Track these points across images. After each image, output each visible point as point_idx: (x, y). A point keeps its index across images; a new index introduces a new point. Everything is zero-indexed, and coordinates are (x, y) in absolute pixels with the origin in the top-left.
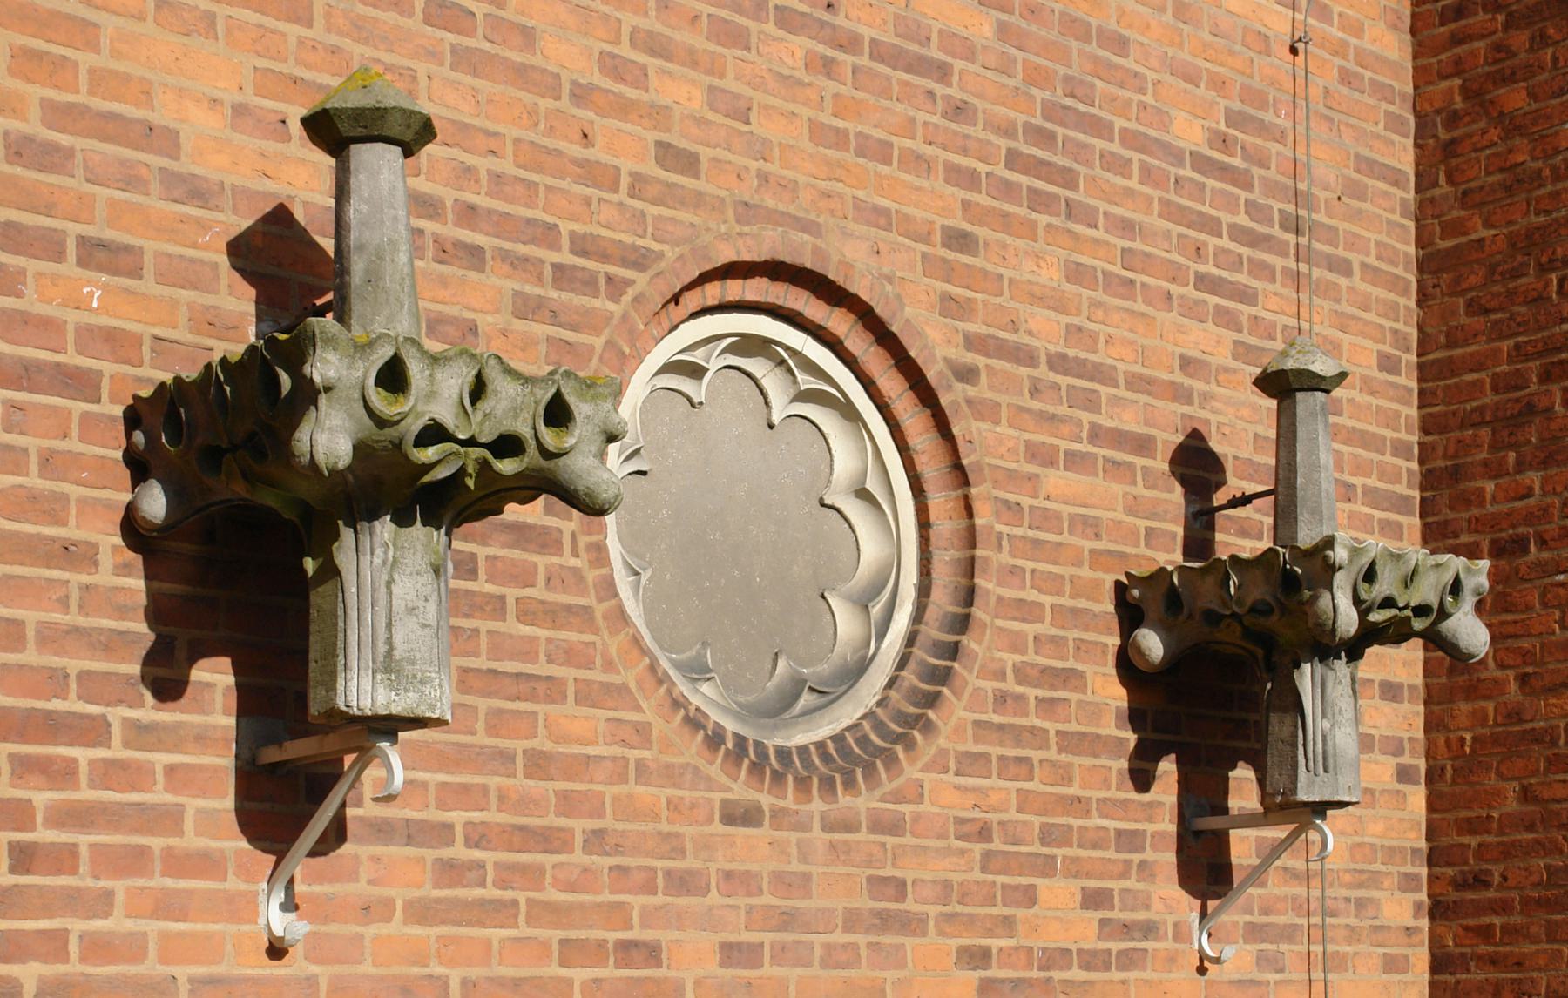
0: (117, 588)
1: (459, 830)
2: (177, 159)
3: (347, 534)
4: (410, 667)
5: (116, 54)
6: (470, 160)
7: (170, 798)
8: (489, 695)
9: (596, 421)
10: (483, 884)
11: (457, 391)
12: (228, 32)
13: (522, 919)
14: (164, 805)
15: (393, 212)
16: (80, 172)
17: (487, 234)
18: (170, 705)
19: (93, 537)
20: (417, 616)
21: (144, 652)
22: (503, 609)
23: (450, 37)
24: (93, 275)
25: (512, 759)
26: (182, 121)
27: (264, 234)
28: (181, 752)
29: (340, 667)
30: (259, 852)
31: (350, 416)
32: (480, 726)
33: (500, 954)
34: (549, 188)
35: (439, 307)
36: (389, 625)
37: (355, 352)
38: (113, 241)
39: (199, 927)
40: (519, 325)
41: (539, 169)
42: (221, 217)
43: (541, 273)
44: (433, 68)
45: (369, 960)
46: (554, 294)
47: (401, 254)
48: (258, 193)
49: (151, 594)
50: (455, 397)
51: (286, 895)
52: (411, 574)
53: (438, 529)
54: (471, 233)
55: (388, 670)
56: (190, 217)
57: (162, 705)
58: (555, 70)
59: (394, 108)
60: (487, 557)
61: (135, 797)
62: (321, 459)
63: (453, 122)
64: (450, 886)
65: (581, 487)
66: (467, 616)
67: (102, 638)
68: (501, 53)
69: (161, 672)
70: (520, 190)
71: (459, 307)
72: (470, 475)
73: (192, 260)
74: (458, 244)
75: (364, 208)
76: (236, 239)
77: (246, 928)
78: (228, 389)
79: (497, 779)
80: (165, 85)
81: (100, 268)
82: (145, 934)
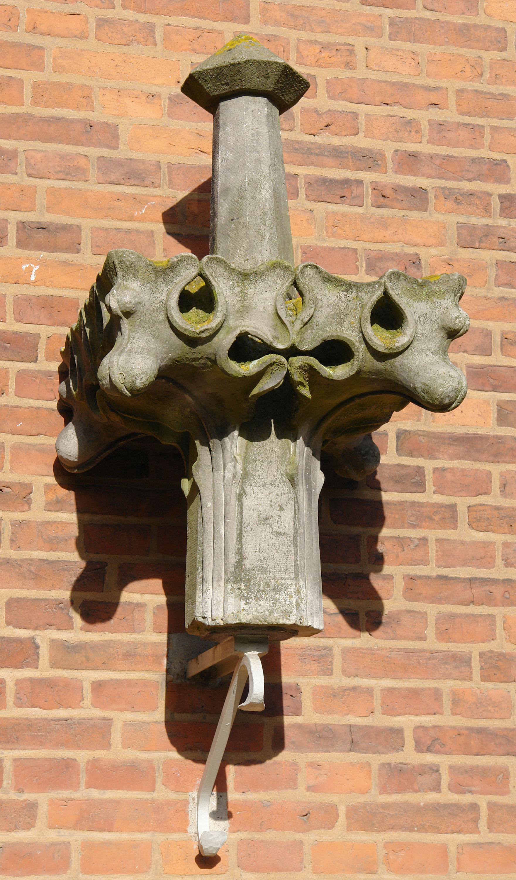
0: (48, 522)
1: (408, 735)
2: (116, 148)
3: (203, 452)
4: (262, 576)
5: (58, 69)
6: (409, 114)
7: (98, 713)
8: (439, 601)
9: (434, 318)
10: (437, 788)
11: (272, 303)
12: (166, 37)
13: (483, 824)
14: (91, 719)
15: (256, 155)
16: (22, 169)
17: (430, 177)
18: (99, 626)
19: (26, 479)
20: (270, 525)
21: (74, 579)
22: (454, 518)
23: (389, 12)
24: (33, 253)
25: (468, 662)
26: (121, 116)
27: (199, 201)
28: (110, 669)
29: (198, 581)
30: (190, 762)
31: (157, 338)
32: (430, 632)
33: (458, 860)
34: (494, 129)
35: (380, 246)
36: (240, 536)
37: (157, 276)
38: (52, 223)
39: (125, 836)
40: (465, 254)
41: (485, 113)
42: (157, 192)
43: (489, 204)
44: (371, 41)
45: (309, 867)
46: (503, 222)
47: (264, 192)
48: (193, 167)
49: (81, 524)
50: (271, 309)
51: (219, 803)
52: (264, 485)
53: (294, 440)
54: (413, 178)
55: (237, 580)
56: (126, 195)
57: (91, 627)
58: (500, 25)
59: (247, 61)
60: (435, 470)
61: (62, 713)
62: (118, 380)
63: (393, 84)
64: (399, 791)
65: (419, 385)
66: (413, 526)
67: (32, 568)
68: (441, 18)
69: (90, 596)
70: (464, 134)
71: (400, 244)
72: (301, 384)
73: (128, 231)
74: (397, 189)
75: (230, 155)
76: (172, 209)
77: (174, 836)
78: (88, 330)
79: (450, 683)
80: (105, 88)
81: (39, 247)
82: (68, 845)
